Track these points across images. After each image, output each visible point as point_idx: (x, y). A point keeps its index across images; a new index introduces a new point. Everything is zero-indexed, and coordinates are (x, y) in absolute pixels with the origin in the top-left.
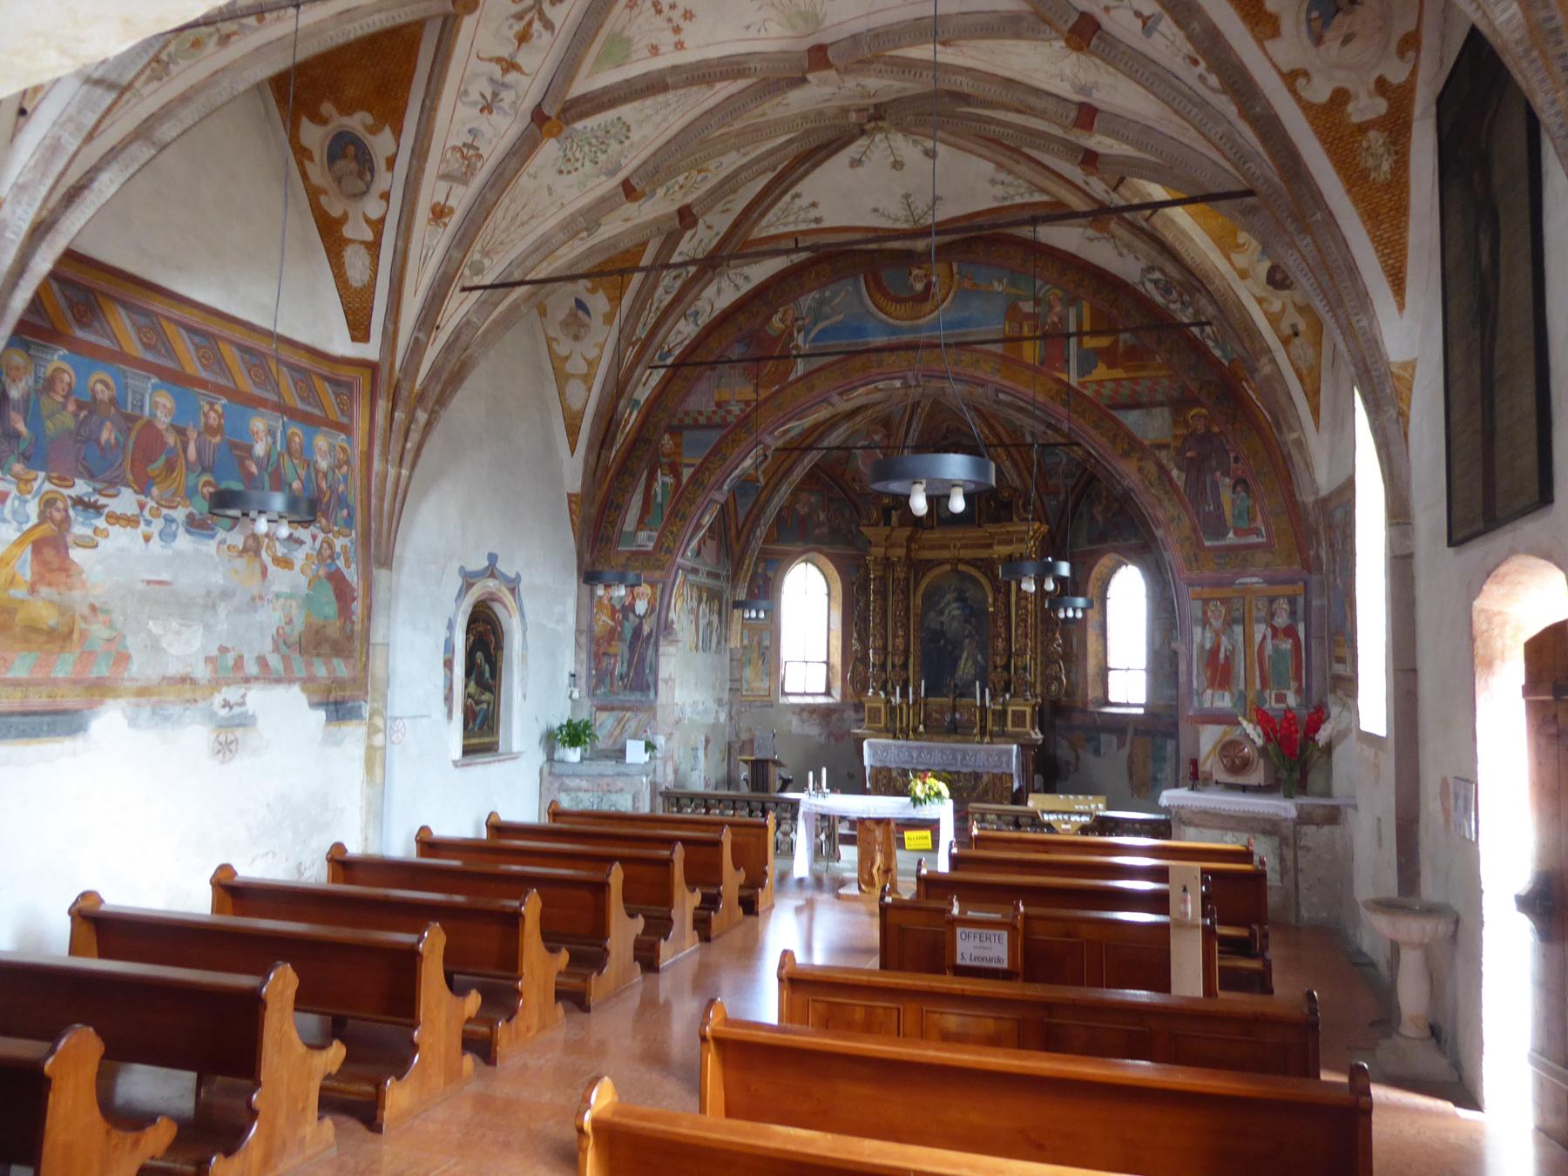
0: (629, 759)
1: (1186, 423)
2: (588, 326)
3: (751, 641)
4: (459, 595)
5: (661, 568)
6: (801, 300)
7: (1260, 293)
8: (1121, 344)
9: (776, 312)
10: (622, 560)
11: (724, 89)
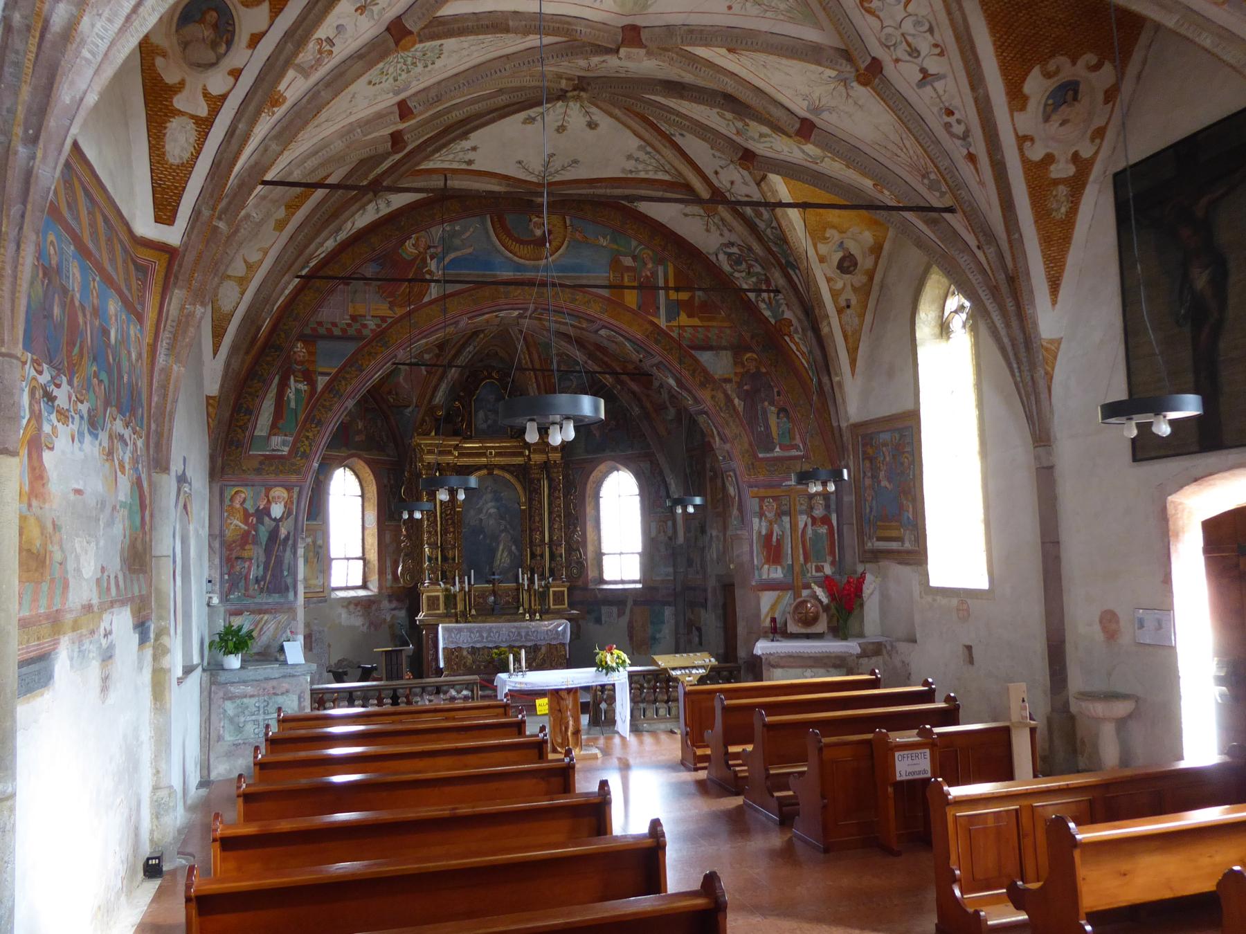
1: (743, 366)
5: (297, 472)
6: (433, 230)
8: (697, 298)
10: (256, 464)
11: (533, 40)
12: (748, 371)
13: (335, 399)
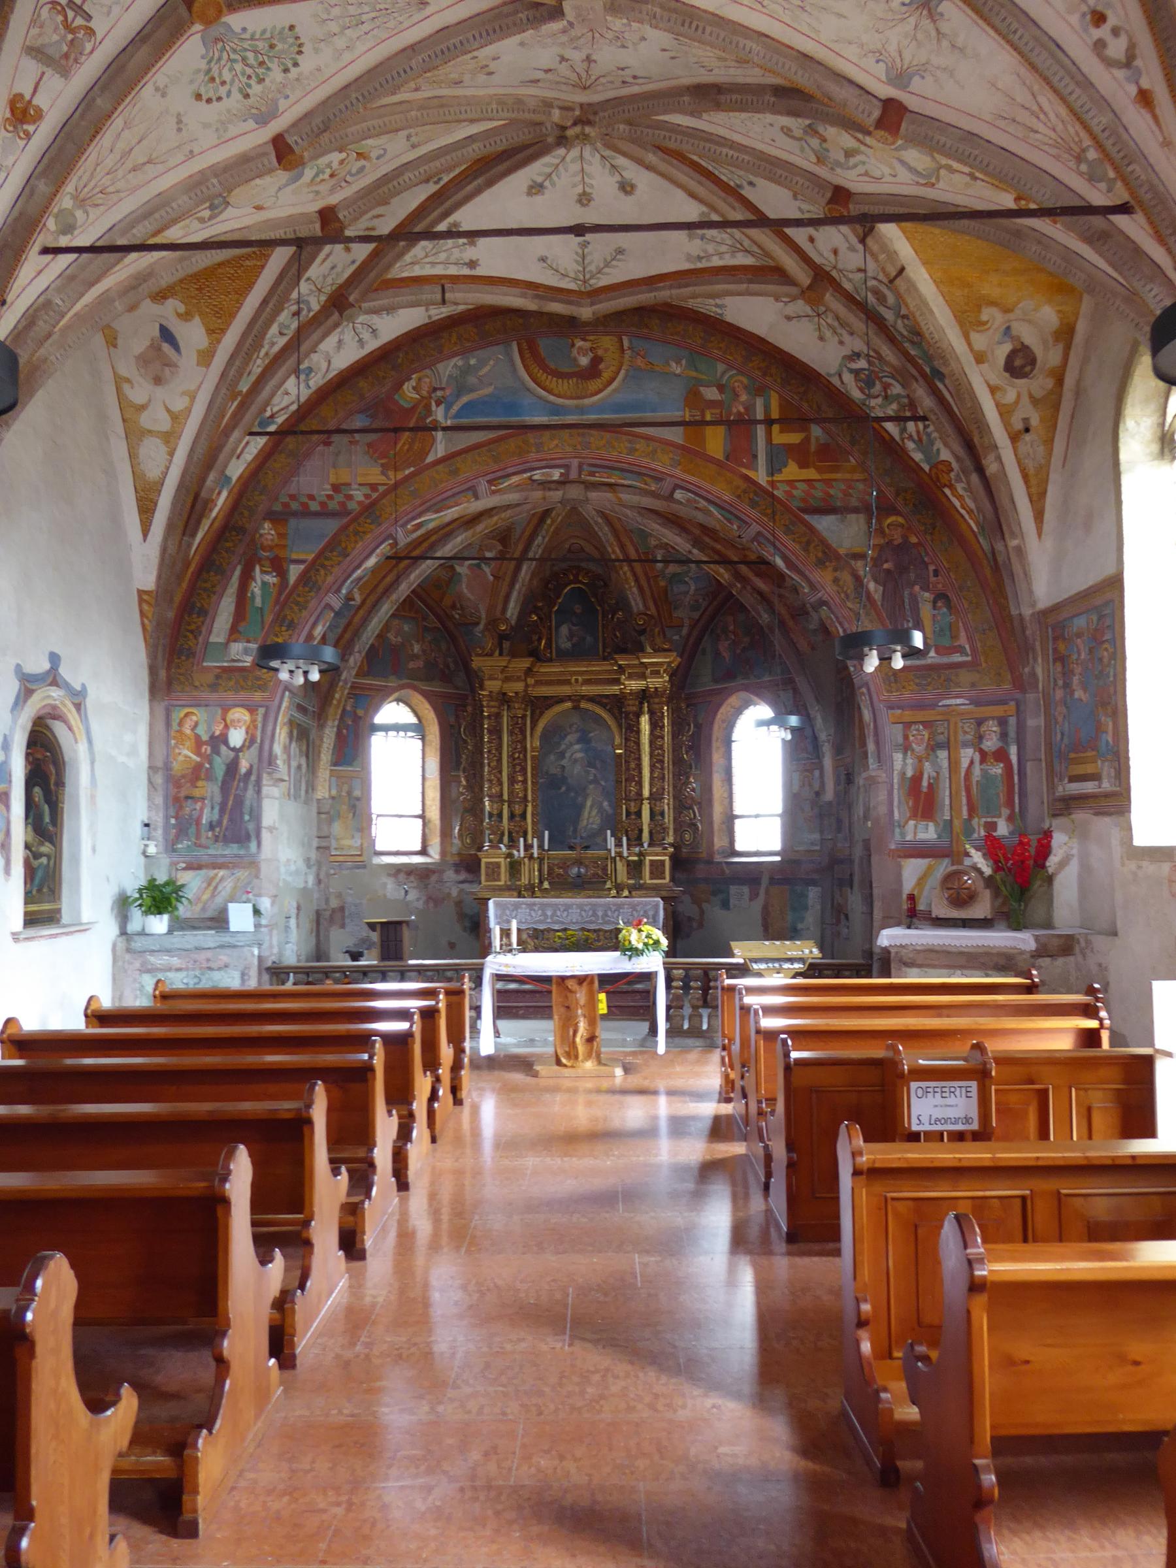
0: (233, 926)
2: (176, 366)
3: (340, 790)
4: (16, 704)
5: (262, 688)
6: (440, 366)
7: (995, 380)
8: (813, 440)
9: (409, 379)
10: (210, 678)
12: (889, 543)
13: (312, 594)
